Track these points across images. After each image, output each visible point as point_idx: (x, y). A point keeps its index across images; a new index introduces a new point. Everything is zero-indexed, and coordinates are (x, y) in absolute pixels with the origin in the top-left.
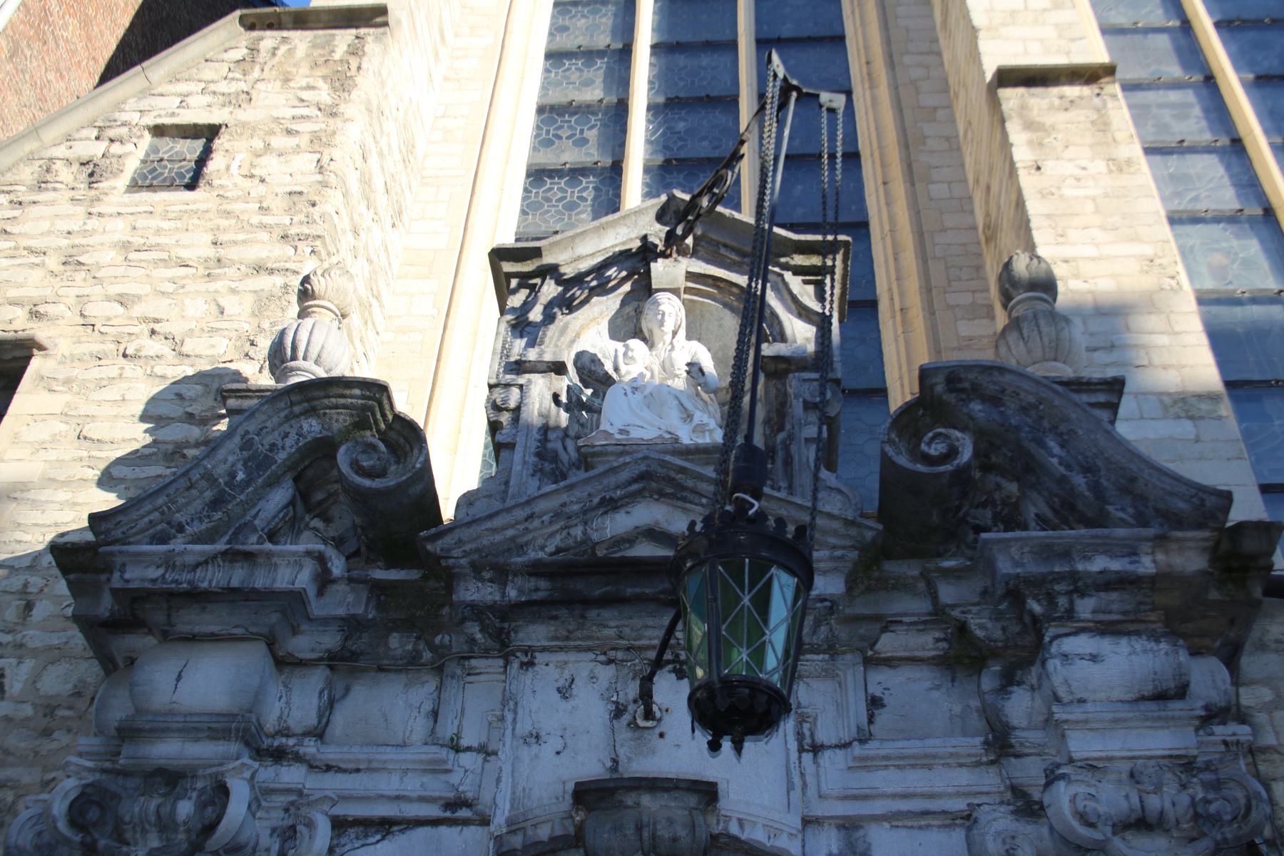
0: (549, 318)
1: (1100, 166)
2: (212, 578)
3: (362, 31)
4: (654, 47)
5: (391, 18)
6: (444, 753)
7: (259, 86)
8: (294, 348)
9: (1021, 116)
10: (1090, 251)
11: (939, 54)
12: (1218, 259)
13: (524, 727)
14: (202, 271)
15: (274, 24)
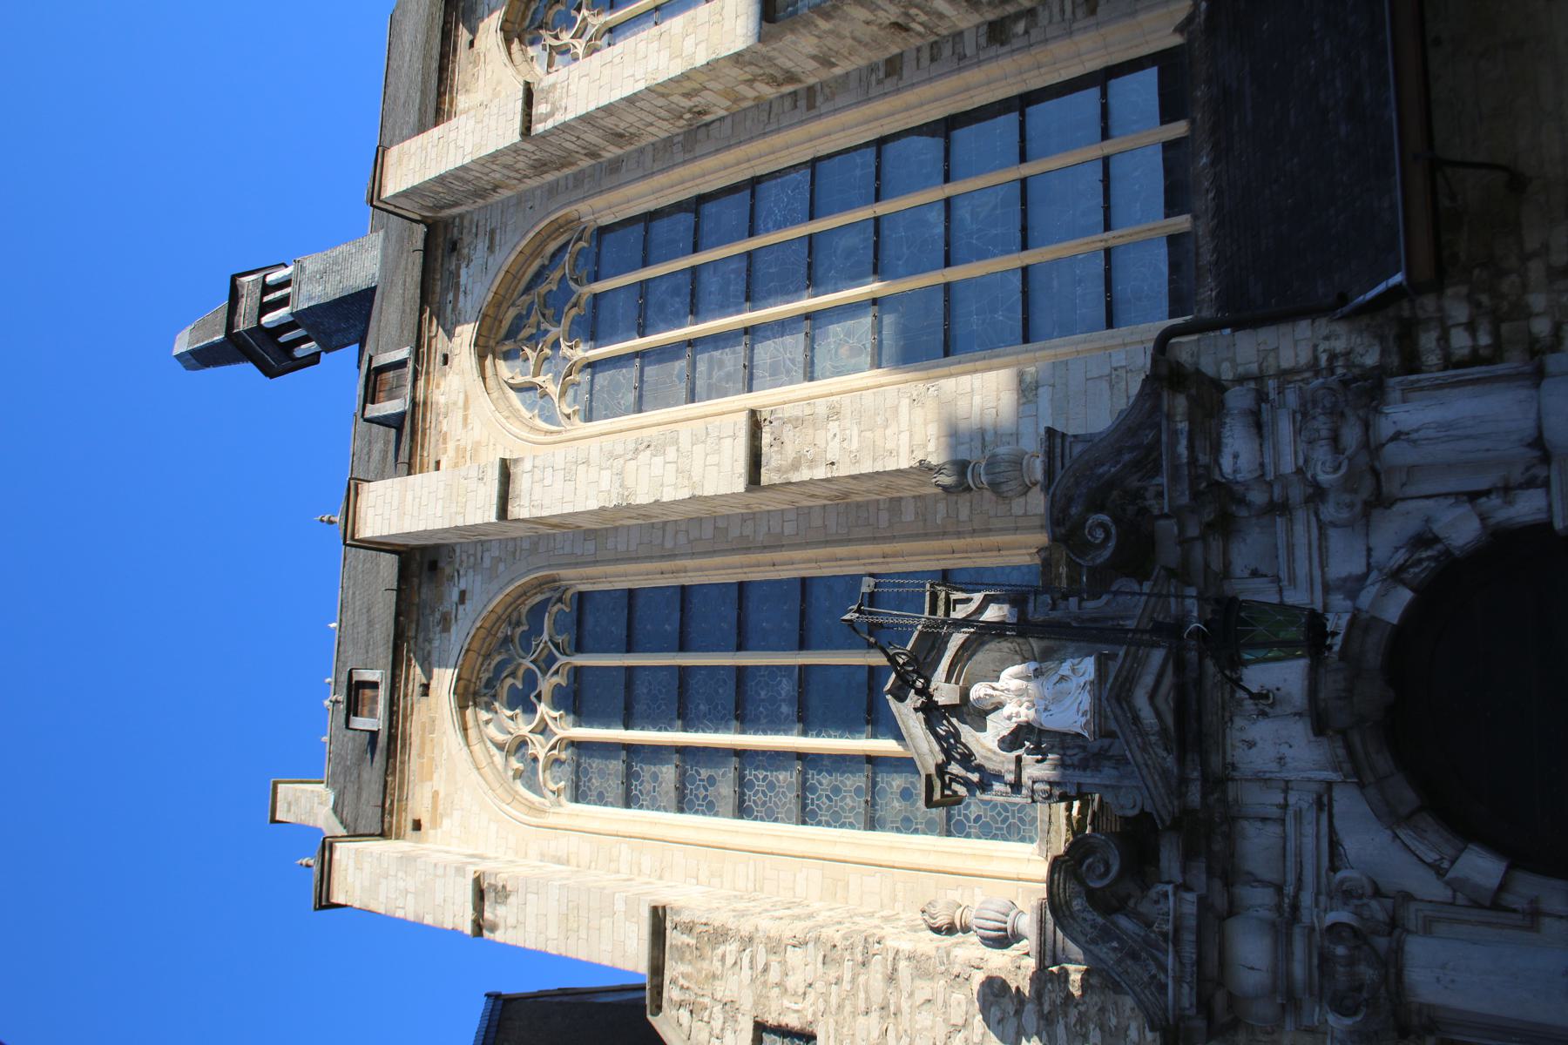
0: (979, 769)
1: (833, 426)
2: (1189, 952)
3: (668, 925)
4: (627, 727)
5: (659, 904)
6: (1290, 812)
7: (718, 996)
8: (999, 930)
9: (786, 472)
10: (905, 437)
11: (665, 523)
12: (844, 351)
13: (1274, 766)
14: (891, 1020)
15: (658, 990)
